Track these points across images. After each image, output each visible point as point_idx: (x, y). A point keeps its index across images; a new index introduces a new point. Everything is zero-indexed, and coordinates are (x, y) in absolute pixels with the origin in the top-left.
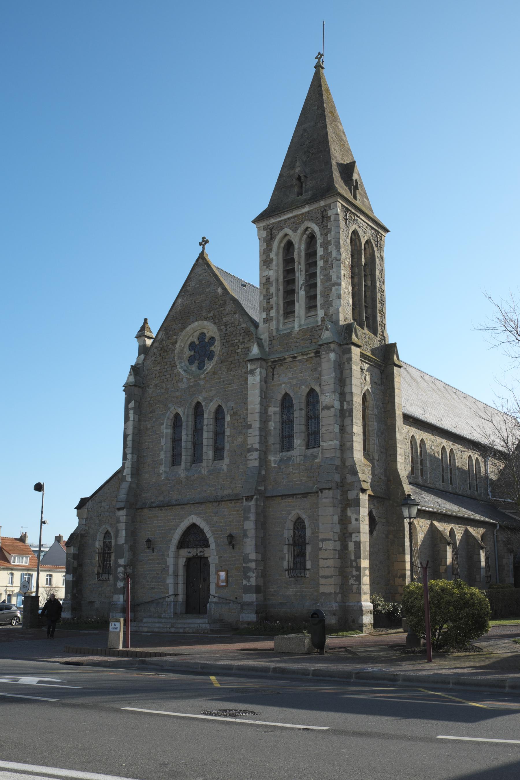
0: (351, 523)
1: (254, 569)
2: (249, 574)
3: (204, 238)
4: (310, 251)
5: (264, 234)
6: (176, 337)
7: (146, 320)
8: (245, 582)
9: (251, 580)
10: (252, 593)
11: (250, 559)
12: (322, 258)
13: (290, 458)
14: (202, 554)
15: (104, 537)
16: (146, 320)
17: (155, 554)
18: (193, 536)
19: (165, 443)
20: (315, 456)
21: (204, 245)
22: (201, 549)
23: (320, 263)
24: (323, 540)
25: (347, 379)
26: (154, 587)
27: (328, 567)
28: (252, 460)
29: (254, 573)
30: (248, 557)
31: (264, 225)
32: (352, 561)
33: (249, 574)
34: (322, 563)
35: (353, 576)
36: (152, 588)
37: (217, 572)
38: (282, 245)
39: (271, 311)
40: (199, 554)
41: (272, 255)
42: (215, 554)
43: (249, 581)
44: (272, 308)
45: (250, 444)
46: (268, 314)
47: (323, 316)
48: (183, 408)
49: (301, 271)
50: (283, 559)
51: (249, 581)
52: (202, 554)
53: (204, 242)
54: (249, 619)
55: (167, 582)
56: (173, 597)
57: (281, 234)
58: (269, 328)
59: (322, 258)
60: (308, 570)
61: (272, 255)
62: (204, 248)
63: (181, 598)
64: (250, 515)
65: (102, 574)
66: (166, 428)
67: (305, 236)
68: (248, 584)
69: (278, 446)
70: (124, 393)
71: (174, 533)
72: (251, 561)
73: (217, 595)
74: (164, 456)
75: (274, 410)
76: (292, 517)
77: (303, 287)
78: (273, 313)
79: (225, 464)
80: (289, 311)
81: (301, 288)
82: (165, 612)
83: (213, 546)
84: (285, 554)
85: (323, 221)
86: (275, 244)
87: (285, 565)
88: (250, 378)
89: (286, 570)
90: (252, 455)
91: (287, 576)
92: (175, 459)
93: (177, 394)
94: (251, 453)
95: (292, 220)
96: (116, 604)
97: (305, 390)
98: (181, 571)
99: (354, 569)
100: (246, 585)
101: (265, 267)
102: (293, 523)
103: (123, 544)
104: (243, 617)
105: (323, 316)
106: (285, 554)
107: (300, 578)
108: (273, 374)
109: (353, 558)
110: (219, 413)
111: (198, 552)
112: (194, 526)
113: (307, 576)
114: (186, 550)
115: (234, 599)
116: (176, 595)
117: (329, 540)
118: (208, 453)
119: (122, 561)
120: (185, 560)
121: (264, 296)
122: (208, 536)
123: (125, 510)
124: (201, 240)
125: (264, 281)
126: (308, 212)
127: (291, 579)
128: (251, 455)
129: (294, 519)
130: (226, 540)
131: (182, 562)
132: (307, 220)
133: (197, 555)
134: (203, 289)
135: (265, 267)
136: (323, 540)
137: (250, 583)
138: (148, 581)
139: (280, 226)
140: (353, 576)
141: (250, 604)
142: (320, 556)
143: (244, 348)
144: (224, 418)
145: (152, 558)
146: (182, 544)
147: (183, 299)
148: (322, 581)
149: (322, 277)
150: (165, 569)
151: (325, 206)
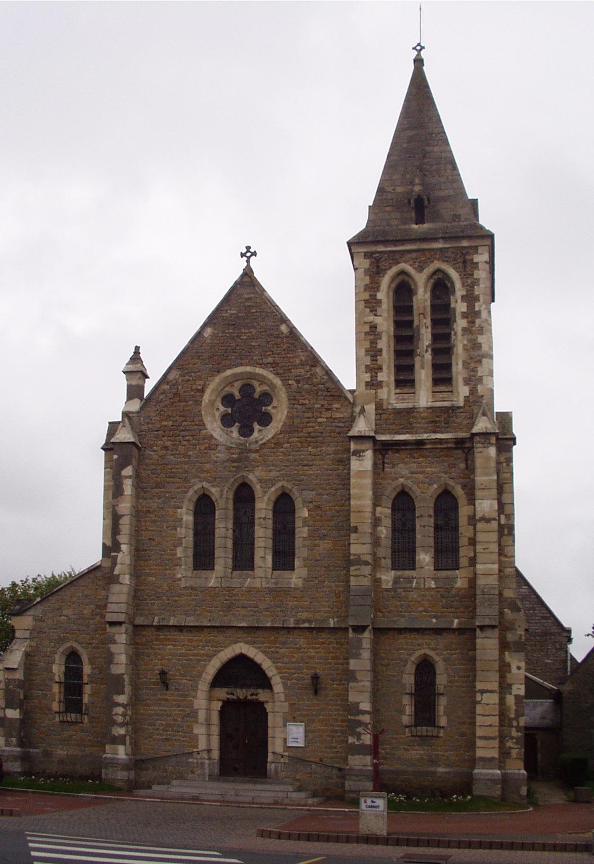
0: (510, 672)
3: (248, 248)
4: (439, 302)
5: (366, 263)
6: (202, 382)
7: (137, 348)
8: (351, 740)
9: (362, 737)
10: (365, 754)
12: (464, 315)
13: (410, 580)
14: (254, 697)
16: (137, 348)
18: (240, 672)
19: (186, 533)
20: (410, 580)
21: (249, 258)
22: (252, 691)
23: (460, 324)
24: (483, 692)
25: (505, 486)
27: (491, 726)
31: (365, 250)
32: (511, 720)
33: (358, 730)
34: (479, 720)
35: (512, 738)
36: (167, 739)
38: (393, 285)
39: (379, 374)
41: (380, 295)
42: (283, 699)
43: (359, 739)
44: (380, 368)
45: (355, 555)
46: (473, 391)
47: (468, 394)
48: (218, 489)
49: (427, 328)
50: (401, 712)
51: (359, 739)
52: (254, 697)
53: (248, 254)
55: (196, 731)
57: (394, 270)
58: (376, 397)
59: (464, 315)
60: (443, 727)
61: (380, 295)
62: (248, 261)
63: (216, 754)
66: (187, 513)
67: (432, 281)
69: (389, 562)
70: (103, 452)
71: (205, 665)
72: (364, 712)
73: (287, 754)
74: (184, 552)
75: (385, 511)
77: (430, 350)
78: (382, 376)
79: (296, 578)
80: (405, 379)
81: (427, 351)
83: (278, 687)
85: (465, 267)
86: (385, 281)
87: (406, 719)
88: (355, 464)
89: (406, 727)
92: (203, 558)
93: (207, 466)
94: (357, 567)
95: (414, 255)
97: (434, 489)
98: (215, 719)
99: (514, 729)
100: (353, 744)
101: (368, 310)
102: (415, 666)
103: (123, 674)
105: (468, 394)
108: (383, 463)
109: (512, 716)
110: (284, 506)
112: (242, 658)
114: (226, 690)
115: (318, 760)
116: (209, 751)
117: (492, 692)
118: (263, 556)
119: (122, 699)
120: (220, 704)
121: (367, 351)
122: (269, 674)
124: (244, 251)
125: (367, 328)
126: (441, 249)
129: (273, 682)
130: (308, 681)
131: (217, 705)
132: (438, 259)
133: (246, 697)
134: (246, 319)
135: (368, 310)
136: (483, 692)
138: (157, 729)
139: (395, 258)
140: (512, 738)
142: (478, 712)
143: (331, 417)
144: (293, 512)
146: (219, 680)
147: (214, 329)
148: (479, 743)
149: (465, 342)
150: (194, 714)
151: (470, 247)
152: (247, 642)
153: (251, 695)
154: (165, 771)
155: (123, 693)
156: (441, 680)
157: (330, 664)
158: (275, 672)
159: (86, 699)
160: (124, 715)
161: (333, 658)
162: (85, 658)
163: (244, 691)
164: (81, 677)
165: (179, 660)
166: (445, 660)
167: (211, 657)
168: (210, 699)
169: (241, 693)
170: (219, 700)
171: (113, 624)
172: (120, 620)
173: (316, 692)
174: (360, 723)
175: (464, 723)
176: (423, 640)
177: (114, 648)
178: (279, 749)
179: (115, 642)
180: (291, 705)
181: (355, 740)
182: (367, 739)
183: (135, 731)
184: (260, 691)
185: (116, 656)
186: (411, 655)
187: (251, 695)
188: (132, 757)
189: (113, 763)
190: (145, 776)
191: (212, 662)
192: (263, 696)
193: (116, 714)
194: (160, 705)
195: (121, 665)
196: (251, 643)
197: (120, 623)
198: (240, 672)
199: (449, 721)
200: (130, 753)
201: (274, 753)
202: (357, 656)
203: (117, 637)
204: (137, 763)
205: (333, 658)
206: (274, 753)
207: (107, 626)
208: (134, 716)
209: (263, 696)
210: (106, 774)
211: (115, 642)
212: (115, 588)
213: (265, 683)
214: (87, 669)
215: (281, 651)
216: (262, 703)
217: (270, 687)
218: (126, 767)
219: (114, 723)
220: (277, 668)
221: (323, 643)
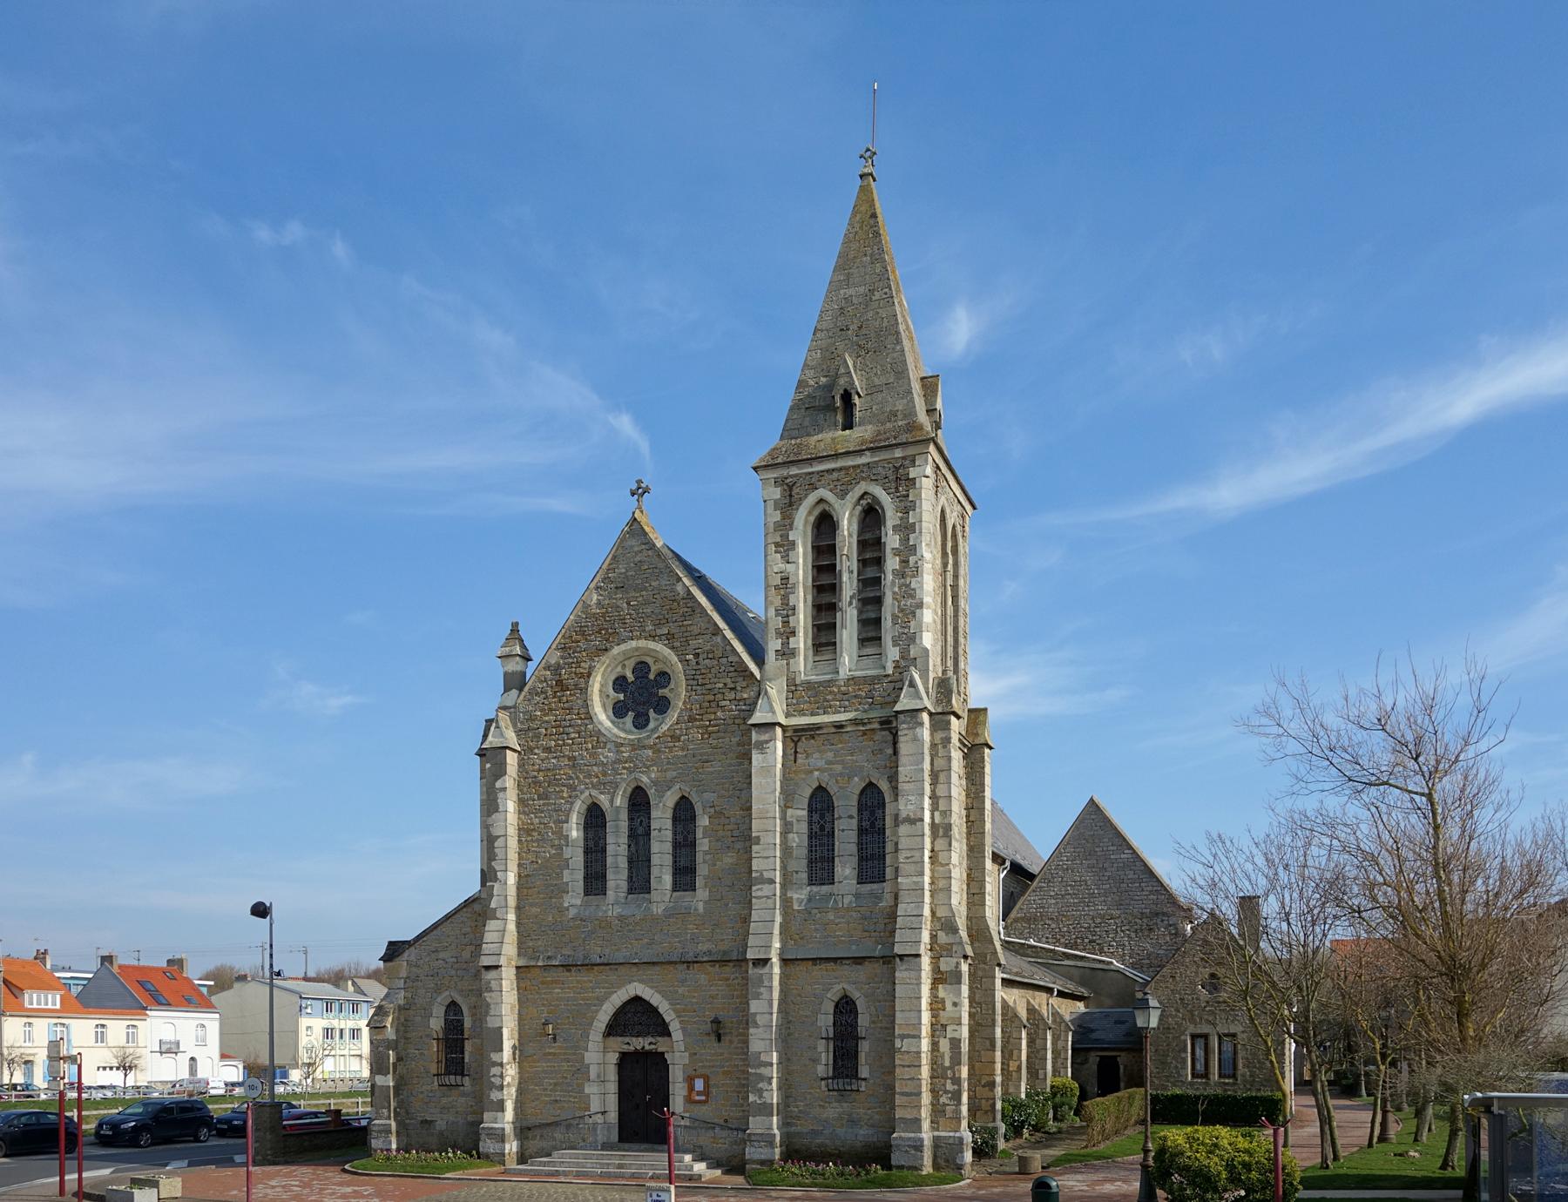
43: (761, 1097)
51: (761, 1097)
76: (834, 994)
112: (637, 1000)
152: (641, 981)
162: (861, 1005)
167: (601, 1001)
209: (661, 1045)
217: (669, 1035)
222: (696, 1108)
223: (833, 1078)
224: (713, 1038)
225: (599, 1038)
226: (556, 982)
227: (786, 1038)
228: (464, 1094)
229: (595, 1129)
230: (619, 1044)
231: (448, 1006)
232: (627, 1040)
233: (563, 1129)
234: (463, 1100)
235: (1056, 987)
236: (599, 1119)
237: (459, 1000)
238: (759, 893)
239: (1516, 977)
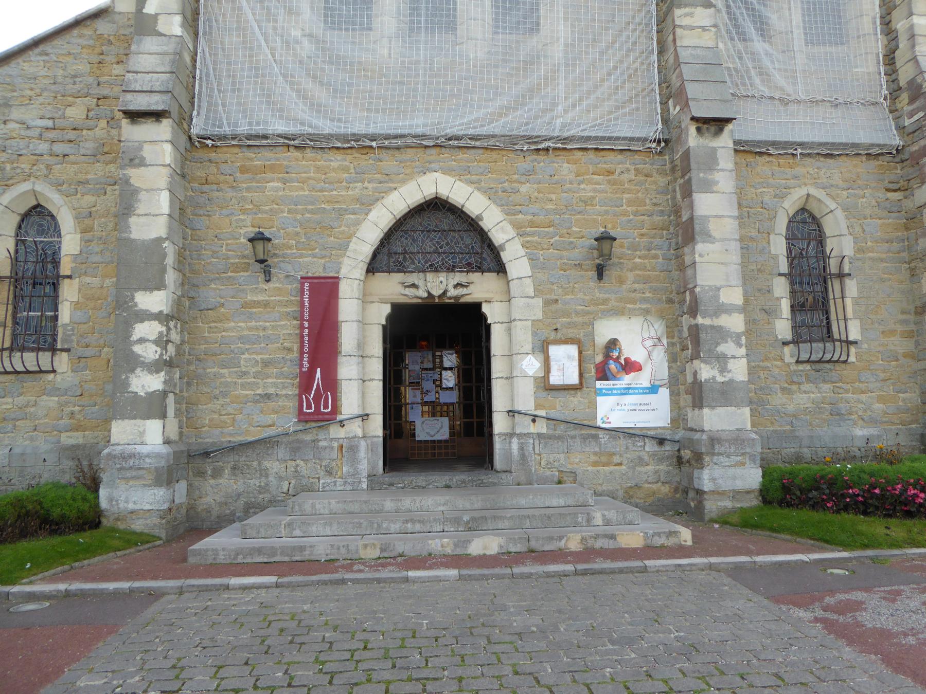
1: (738, 336)
2: (721, 348)
9: (731, 365)
11: (723, 304)
15: (20, 227)
17: (271, 285)
18: (440, 230)
22: (459, 277)
26: (271, 391)
28: (691, 28)
29: (740, 346)
30: (717, 297)
33: (721, 348)
36: (268, 396)
37: (542, 348)
40: (452, 292)
43: (723, 370)
51: (723, 370)
54: (739, 485)
56: (358, 422)
64: (718, 176)
65: (11, 349)
68: (720, 379)
71: (358, 223)
73: (542, 413)
76: (790, 205)
82: (329, 473)
84: (779, 299)
90: (691, 15)
91: (789, 359)
94: (687, 10)
96: (132, 456)
103: (159, 241)
104: (713, 480)
106: (779, 299)
107: (828, 366)
111: (450, 287)
112: (436, 206)
113: (852, 359)
114: (398, 277)
119: (154, 301)
120: (387, 309)
122: (498, 237)
123: (166, 123)
127: (801, 367)
128: (686, 15)
129: (505, 256)
137: (728, 377)
141: (738, 439)
145: (260, 298)
146: (383, 259)
152: (448, 171)
153: (456, 286)
154: (264, 473)
155: (160, 286)
156: (841, 242)
157: (625, 214)
158: (511, 232)
159: (65, 314)
160: (162, 342)
161: (630, 203)
162: (66, 221)
163: (442, 277)
164: (56, 263)
165: (296, 212)
166: (846, 209)
167: (367, 204)
168: (365, 299)
169: (439, 285)
170: (383, 301)
171: (135, 116)
172: (154, 108)
173: (600, 271)
174: (722, 334)
175: (892, 332)
176: (809, 167)
177: (137, 176)
178: (526, 400)
179: (142, 163)
180: (547, 303)
181: (715, 373)
182: (739, 370)
183: (190, 380)
184: (475, 277)
185: (143, 196)
186: (783, 197)
187: (456, 286)
188: (535, 477)
189: (129, 464)
190: (218, 489)
191: (373, 215)
192: (480, 288)
193: (142, 341)
194: (251, 317)
195: (152, 220)
196: (461, 174)
197: (157, 115)
198: (440, 230)
199: (864, 330)
200: (174, 436)
201: (512, 413)
202: (708, 187)
203: (147, 152)
204: (192, 459)
205: (630, 203)
206: (512, 413)
207: (125, 122)
208: (186, 347)
209: (480, 288)
210: (111, 500)
211: (142, 163)
212: (150, 44)
213: (488, 258)
214: (70, 244)
215: (524, 189)
216: (477, 306)
217: (500, 269)
218: (166, 476)
219: (133, 363)
220: (517, 226)
221: (610, 173)
222: (560, 400)
223: (796, 341)
224: (593, 274)
225: (359, 272)
226: (273, 169)
227: (753, 276)
228: (55, 391)
229: (353, 449)
230: (394, 288)
231: (25, 216)
232: (414, 278)
233: (281, 452)
234: (51, 402)
235: (85, 132)
236: (355, 428)
237: (55, 201)
238: (686, 21)
239: (790, 474)
